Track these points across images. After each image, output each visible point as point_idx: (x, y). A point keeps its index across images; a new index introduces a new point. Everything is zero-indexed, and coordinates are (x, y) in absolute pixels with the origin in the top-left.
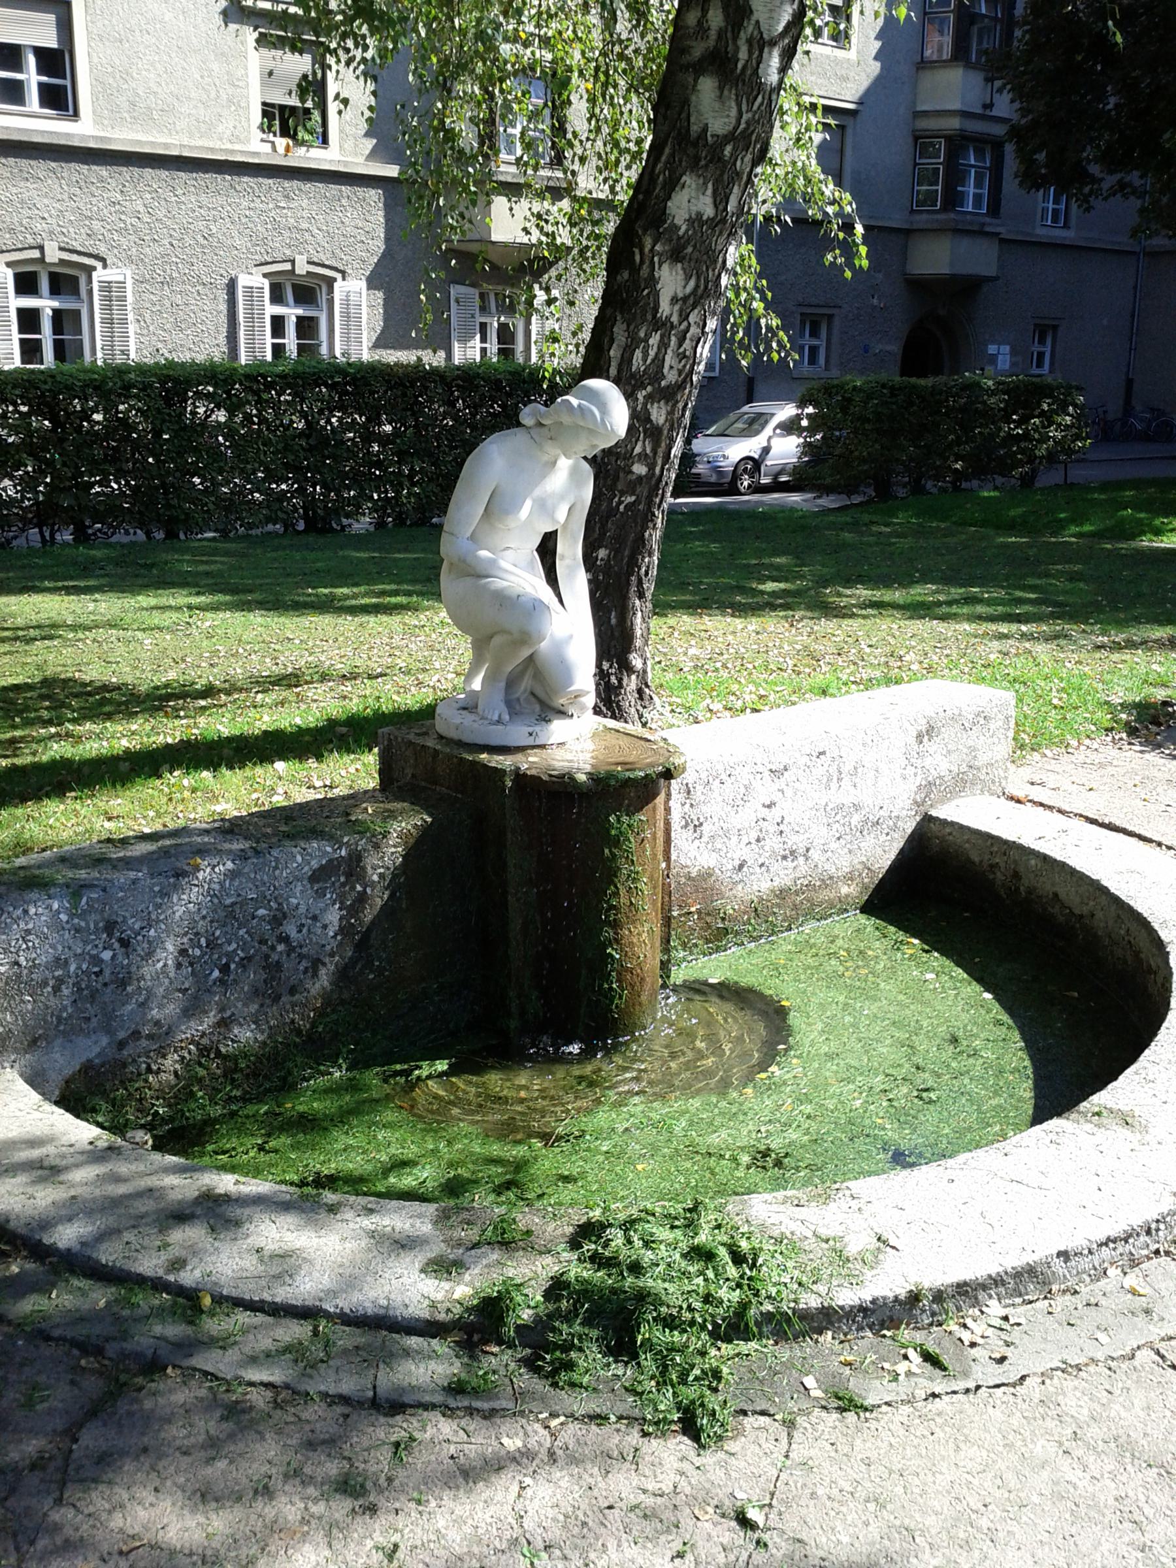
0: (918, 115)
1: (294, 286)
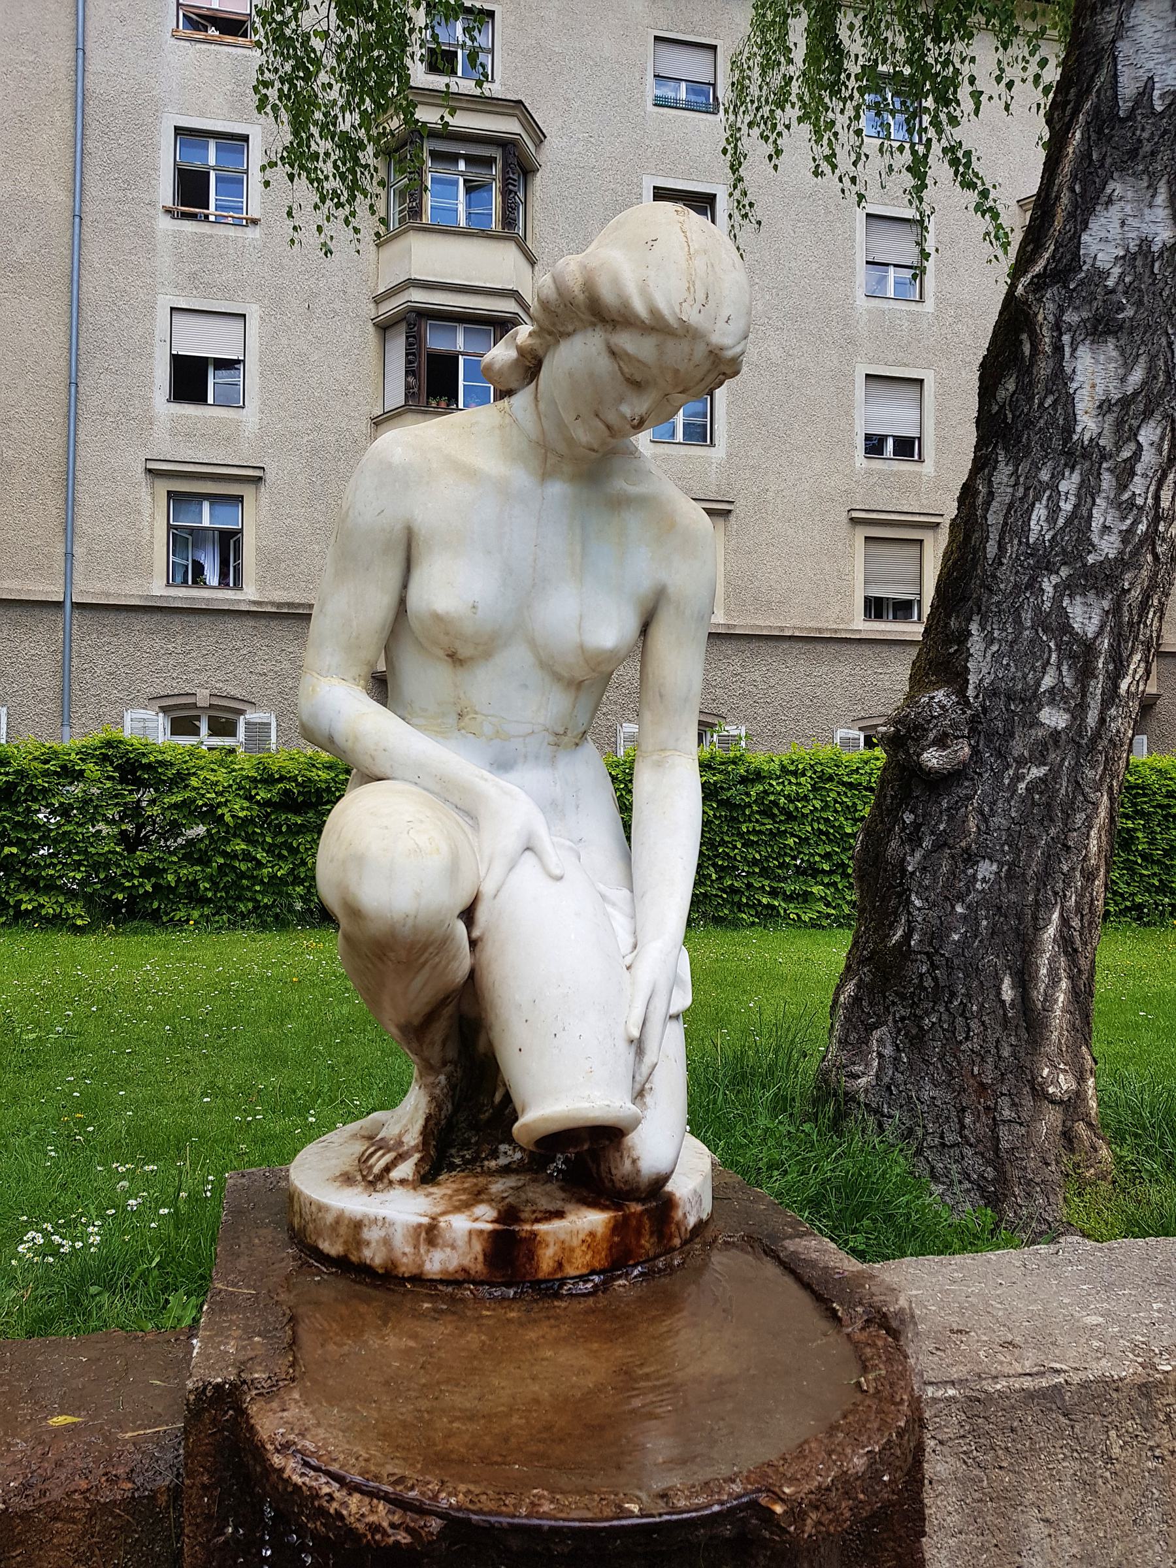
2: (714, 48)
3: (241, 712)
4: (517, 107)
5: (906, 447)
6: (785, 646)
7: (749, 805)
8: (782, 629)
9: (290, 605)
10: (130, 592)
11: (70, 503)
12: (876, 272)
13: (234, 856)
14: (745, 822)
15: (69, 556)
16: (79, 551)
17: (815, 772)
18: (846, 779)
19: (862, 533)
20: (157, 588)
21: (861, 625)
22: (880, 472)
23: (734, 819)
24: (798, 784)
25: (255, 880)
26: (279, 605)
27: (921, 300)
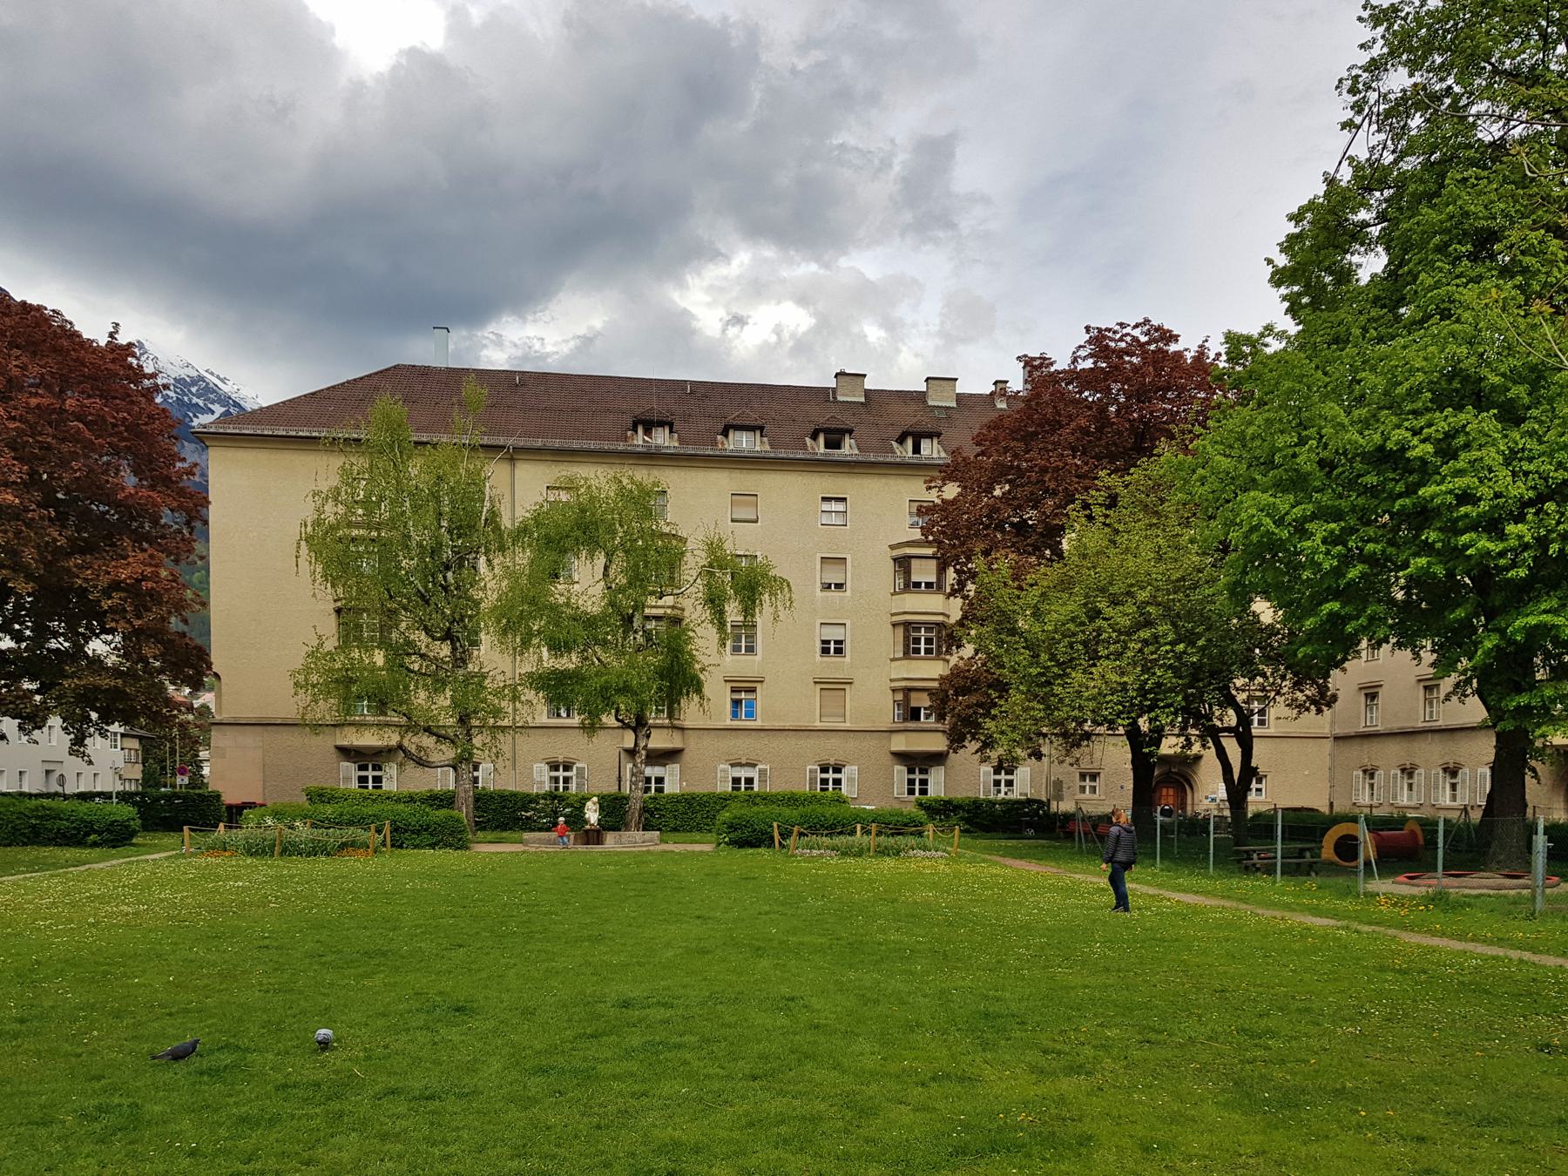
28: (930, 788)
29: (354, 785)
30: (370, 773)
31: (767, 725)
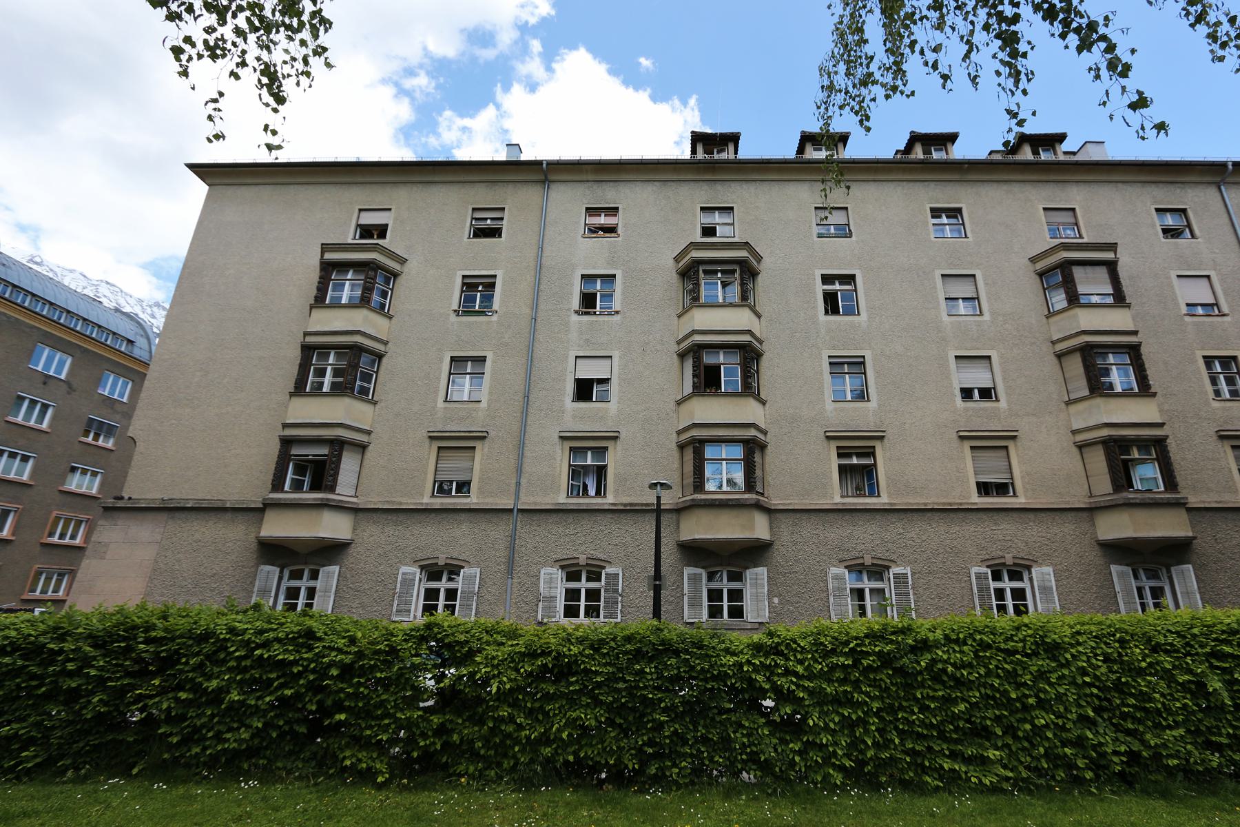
0: (1074, 432)
1: (1008, 571)
2: (846, 208)
3: (604, 568)
4: (746, 245)
5: (986, 393)
6: (929, 514)
7: (920, 673)
8: (925, 504)
9: (631, 504)
10: (546, 502)
11: (521, 456)
12: (951, 303)
13: (501, 720)
14: (919, 687)
15: (518, 484)
16: (523, 481)
17: (974, 640)
18: (1002, 646)
19: (967, 445)
20: (562, 499)
21: (976, 500)
22: (973, 409)
23: (908, 685)
24: (961, 652)
25: (517, 741)
26: (625, 505)
27: (981, 314)
28: (748, 604)
29: (850, 604)
30: (303, 584)
31: (901, 502)
